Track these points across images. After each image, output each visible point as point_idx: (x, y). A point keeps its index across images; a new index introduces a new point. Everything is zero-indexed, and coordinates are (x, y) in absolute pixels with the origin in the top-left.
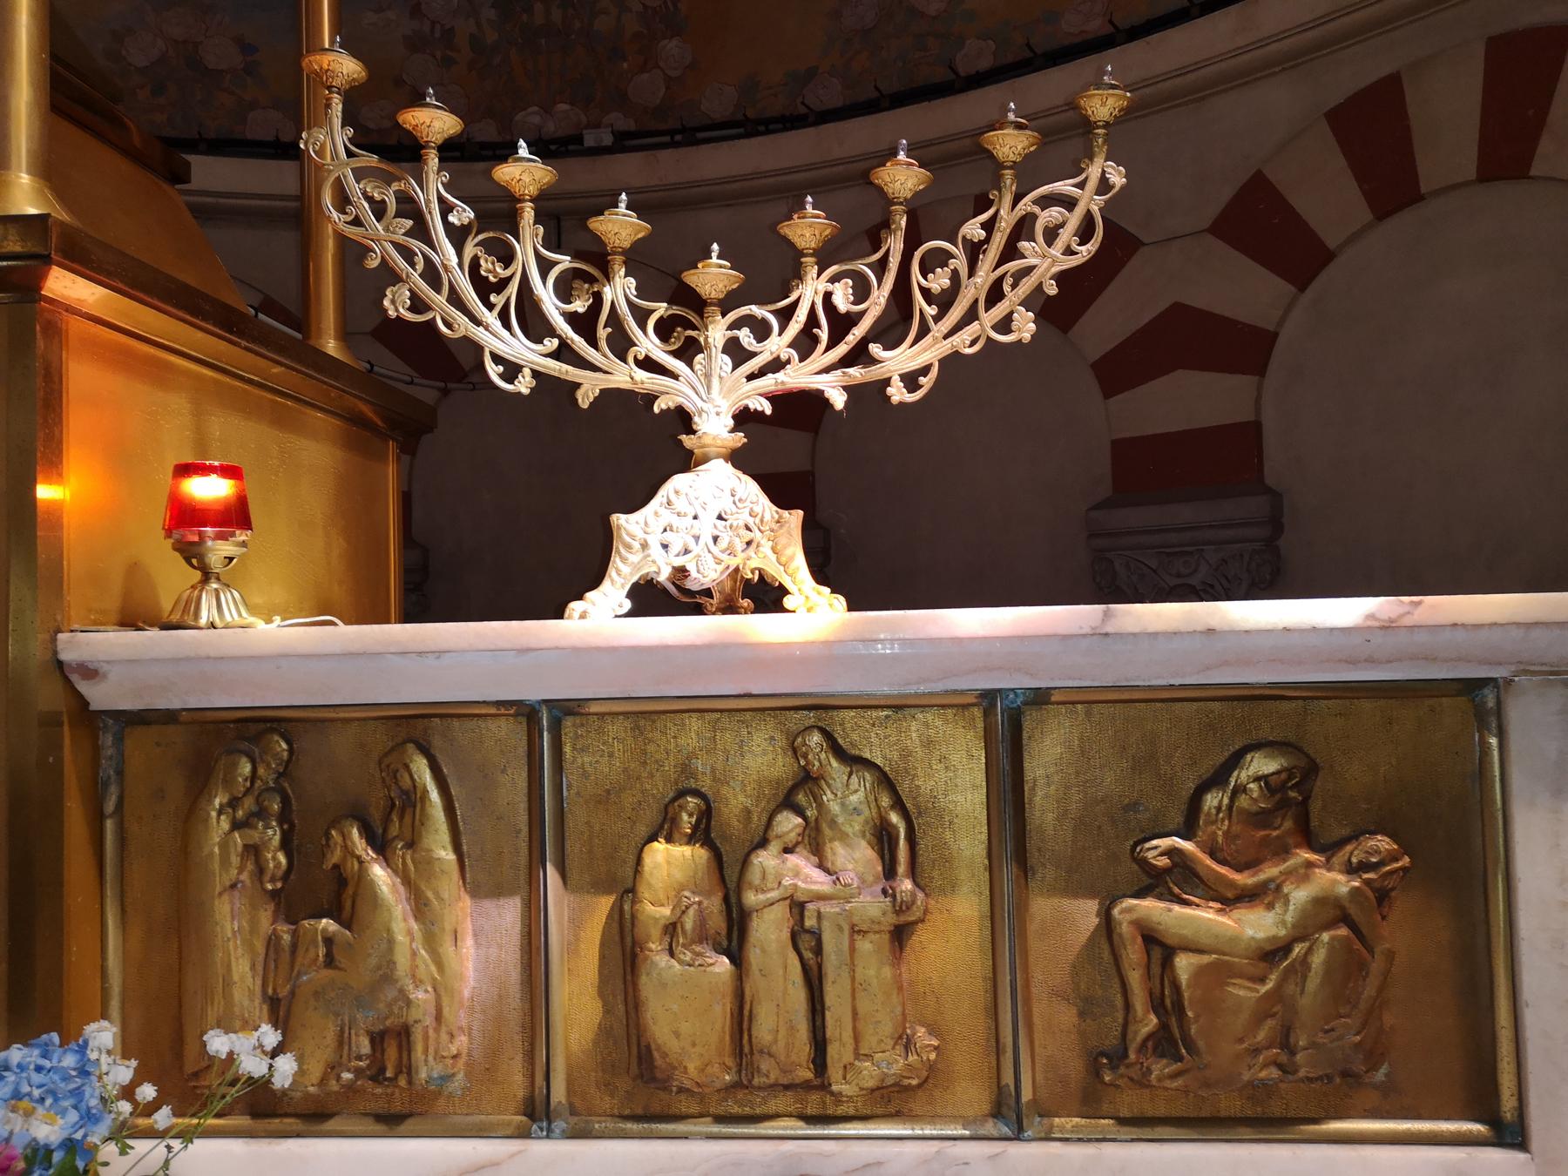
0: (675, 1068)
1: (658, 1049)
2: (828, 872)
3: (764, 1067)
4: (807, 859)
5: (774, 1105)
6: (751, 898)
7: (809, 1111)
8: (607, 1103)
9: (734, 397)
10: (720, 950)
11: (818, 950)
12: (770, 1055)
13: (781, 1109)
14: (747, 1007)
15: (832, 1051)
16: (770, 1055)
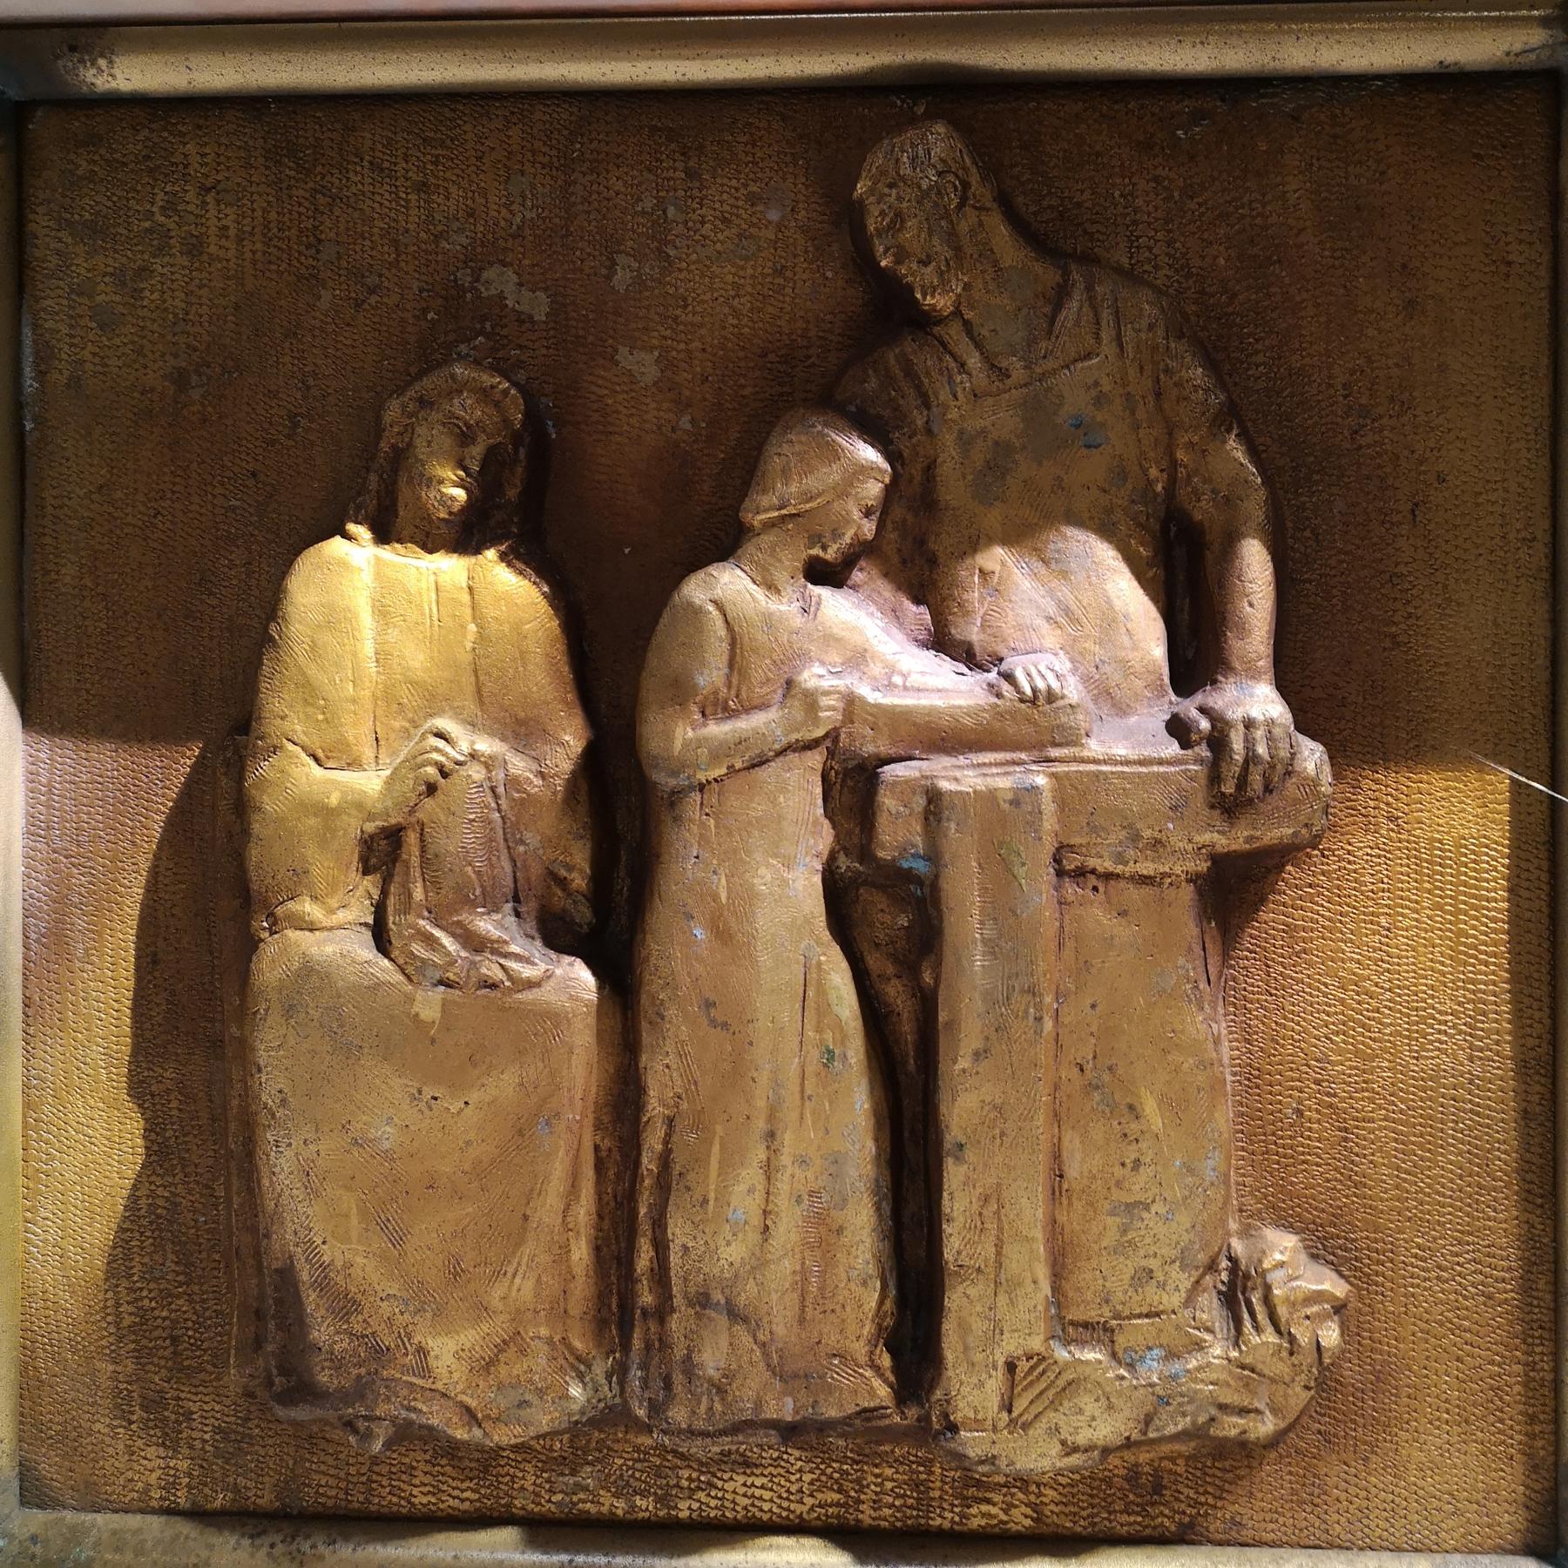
0: (379, 1353)
1: (323, 1285)
2: (967, 656)
3: (711, 1360)
4: (895, 615)
5: (738, 1493)
6: (683, 737)
7: (867, 1515)
8: (152, 1467)
9: (274, 996)
10: (558, 935)
11: (926, 937)
12: (735, 1314)
13: (768, 1508)
14: (653, 1141)
15: (963, 1304)
16: (735, 1314)
